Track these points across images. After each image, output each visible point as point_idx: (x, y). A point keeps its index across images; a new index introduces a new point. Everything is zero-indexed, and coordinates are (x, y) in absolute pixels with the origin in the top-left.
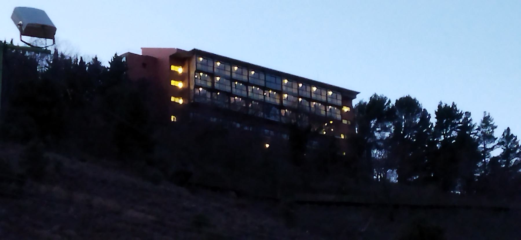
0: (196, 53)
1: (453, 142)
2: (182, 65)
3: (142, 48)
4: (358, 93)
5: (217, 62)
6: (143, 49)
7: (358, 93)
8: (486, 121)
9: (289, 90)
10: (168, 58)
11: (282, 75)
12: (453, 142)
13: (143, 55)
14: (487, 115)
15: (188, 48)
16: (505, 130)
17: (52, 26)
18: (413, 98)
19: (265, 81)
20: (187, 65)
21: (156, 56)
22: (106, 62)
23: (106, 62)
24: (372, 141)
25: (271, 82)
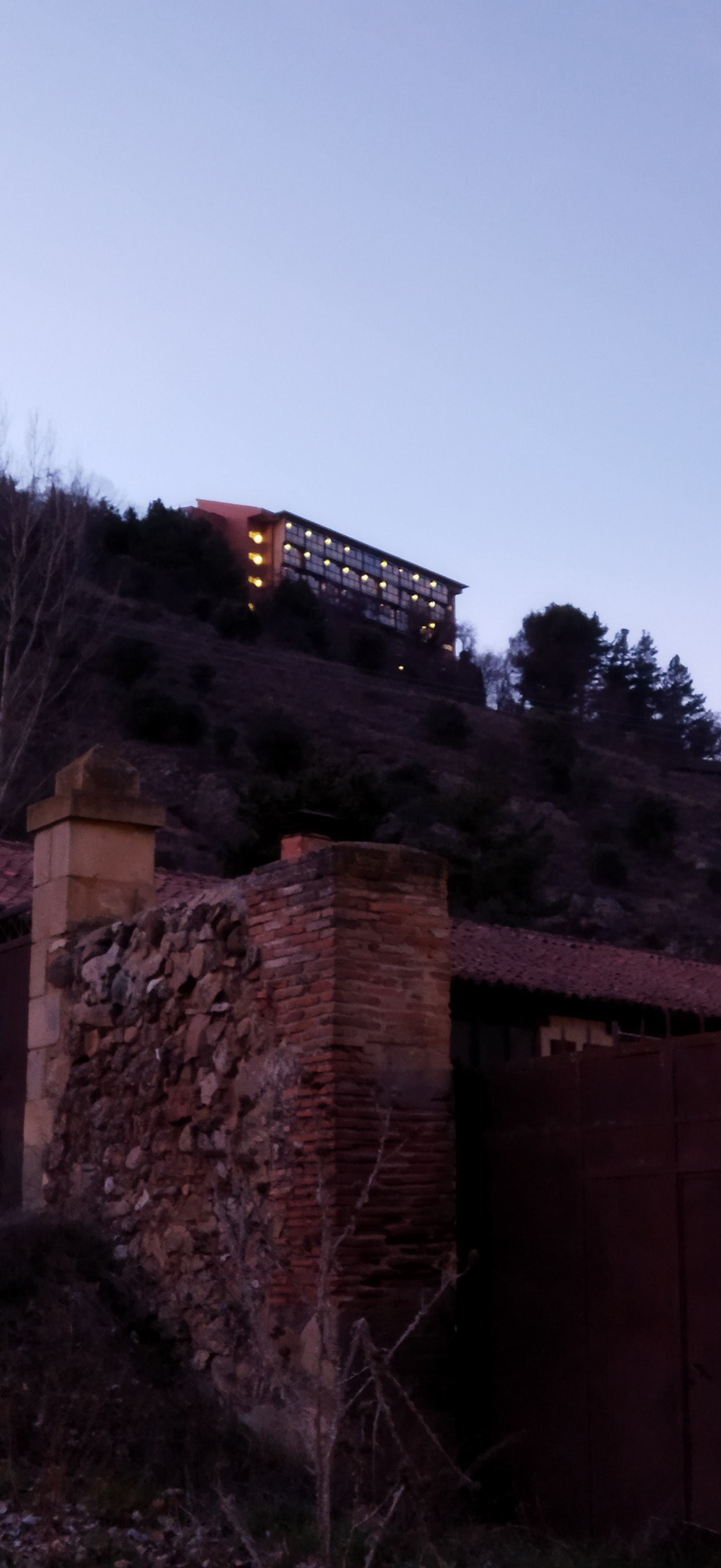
0: (286, 516)
1: (705, 758)
2: (263, 532)
3: (197, 500)
4: (465, 587)
5: (286, 522)
6: (200, 502)
7: (465, 587)
8: (646, 642)
9: (390, 577)
10: (245, 520)
11: (380, 555)
12: (705, 758)
13: (202, 508)
14: (646, 635)
15: (275, 508)
16: (654, 652)
17: (259, 513)
18: (590, 616)
19: (363, 562)
20: (269, 531)
21: (220, 512)
22: (142, 513)
23: (142, 513)
24: (67, 1519)
25: (369, 565)
